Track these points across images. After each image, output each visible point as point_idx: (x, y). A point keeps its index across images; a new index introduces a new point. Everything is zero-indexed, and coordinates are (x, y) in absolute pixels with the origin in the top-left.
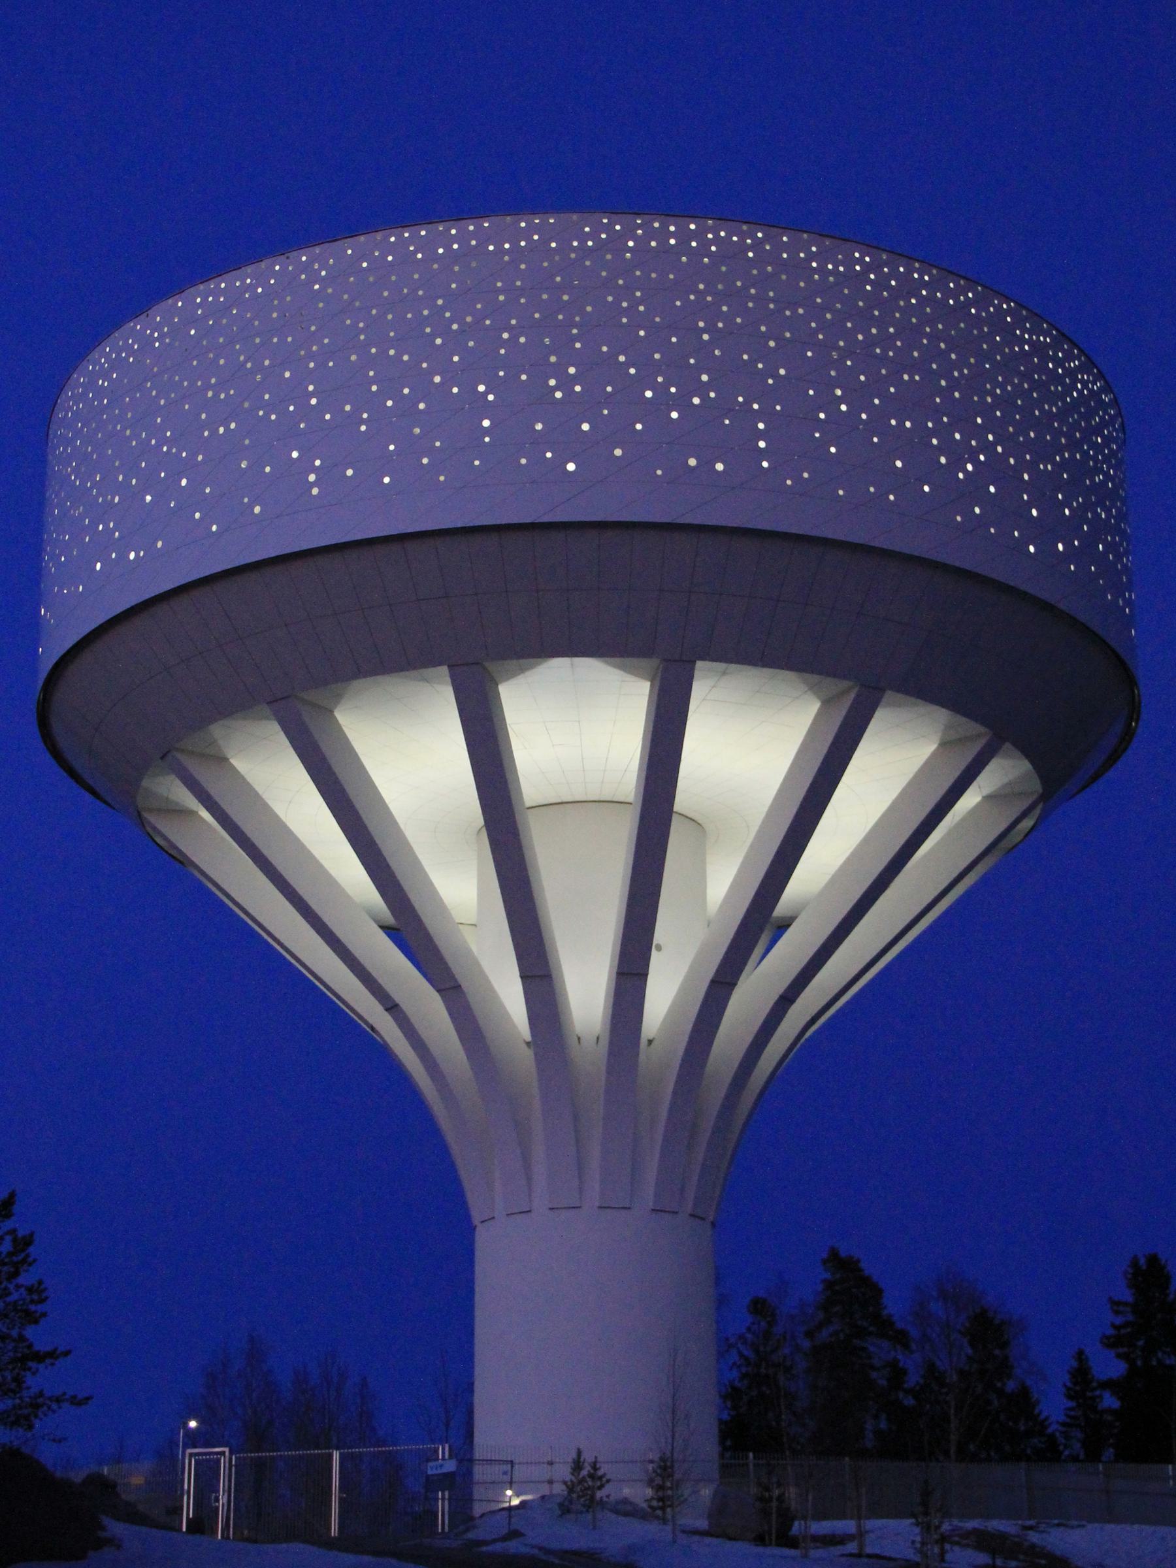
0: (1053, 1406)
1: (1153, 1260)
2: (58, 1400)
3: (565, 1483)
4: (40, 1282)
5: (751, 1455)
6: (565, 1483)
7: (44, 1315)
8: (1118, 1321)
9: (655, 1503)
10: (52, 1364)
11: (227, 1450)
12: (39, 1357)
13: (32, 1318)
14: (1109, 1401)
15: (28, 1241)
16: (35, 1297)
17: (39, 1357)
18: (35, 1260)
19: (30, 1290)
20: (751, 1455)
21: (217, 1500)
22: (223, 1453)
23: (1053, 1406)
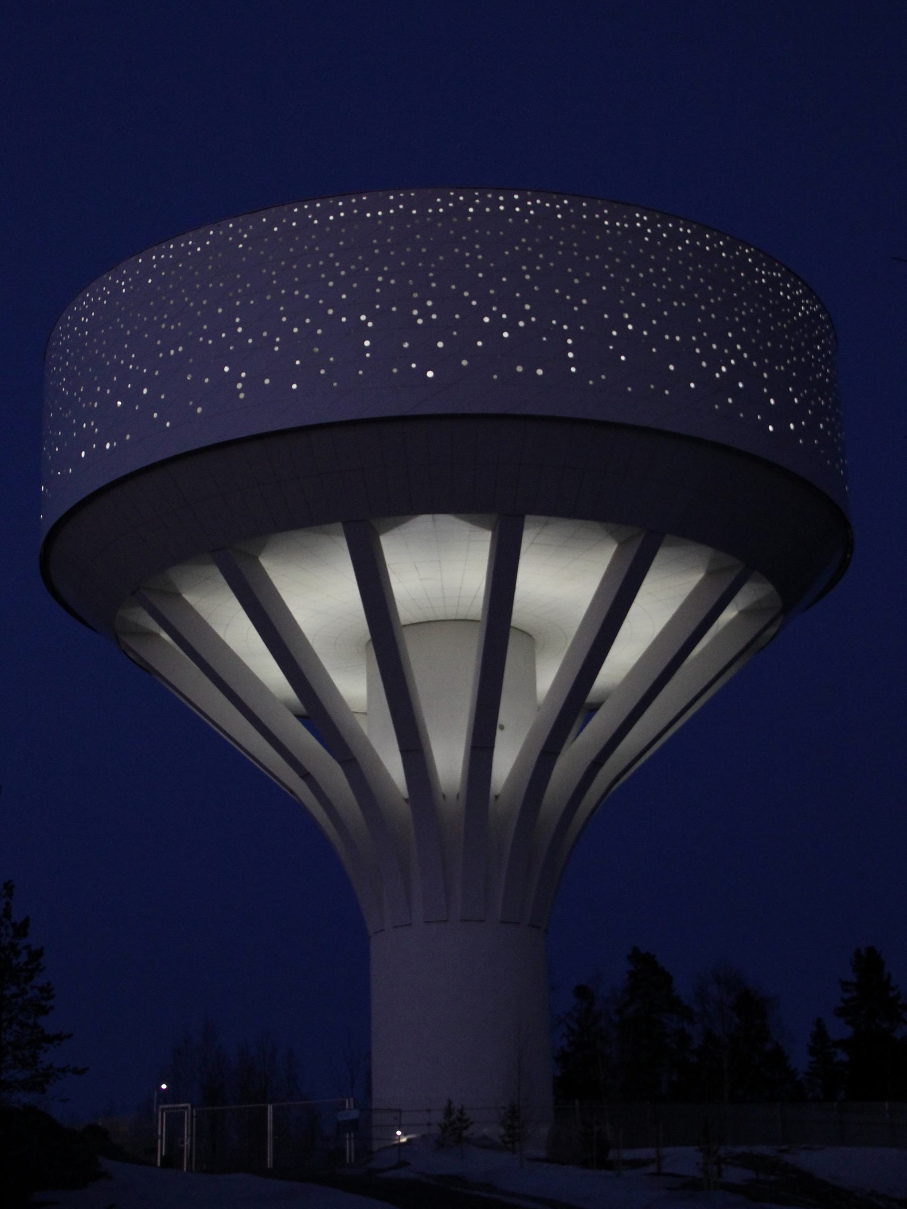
0: (800, 1061)
3: (440, 1125)
5: (577, 1102)
6: (440, 1125)
7: (52, 1008)
9: (507, 1139)
10: (59, 1044)
11: (189, 1105)
14: (842, 1056)
15: (40, 953)
20: (577, 1102)
21: (183, 1142)
22: (186, 1108)
23: (800, 1061)
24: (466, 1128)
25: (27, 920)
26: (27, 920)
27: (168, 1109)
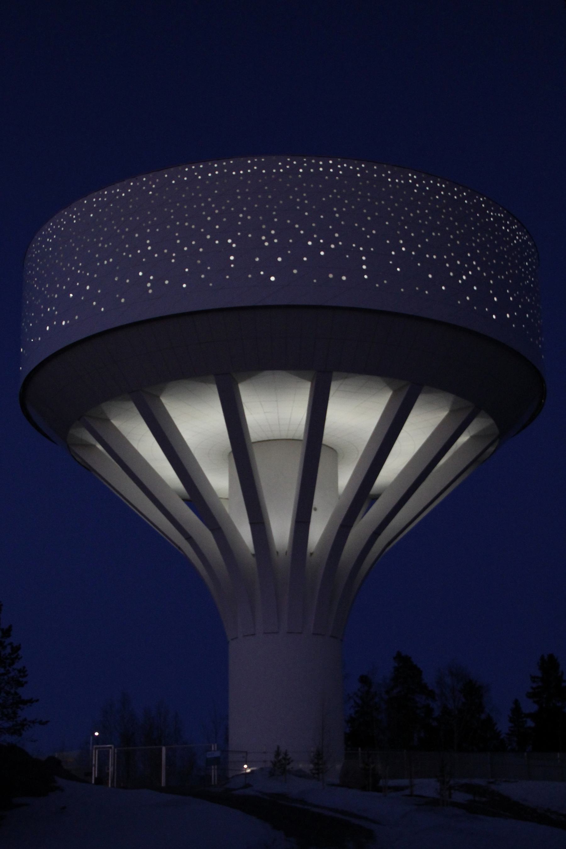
0: (503, 726)
1: (551, 656)
2: (33, 722)
4: (24, 667)
5: (360, 749)
7: (26, 682)
8: (534, 685)
12: (25, 702)
13: (21, 685)
14: (530, 723)
15: (18, 648)
16: (22, 674)
17: (25, 702)
18: (21, 657)
19: (20, 671)
20: (360, 749)
21: (108, 769)
22: (111, 748)
23: (503, 726)
24: (289, 764)
25: (11, 627)
26: (11, 627)
27: (99, 748)
